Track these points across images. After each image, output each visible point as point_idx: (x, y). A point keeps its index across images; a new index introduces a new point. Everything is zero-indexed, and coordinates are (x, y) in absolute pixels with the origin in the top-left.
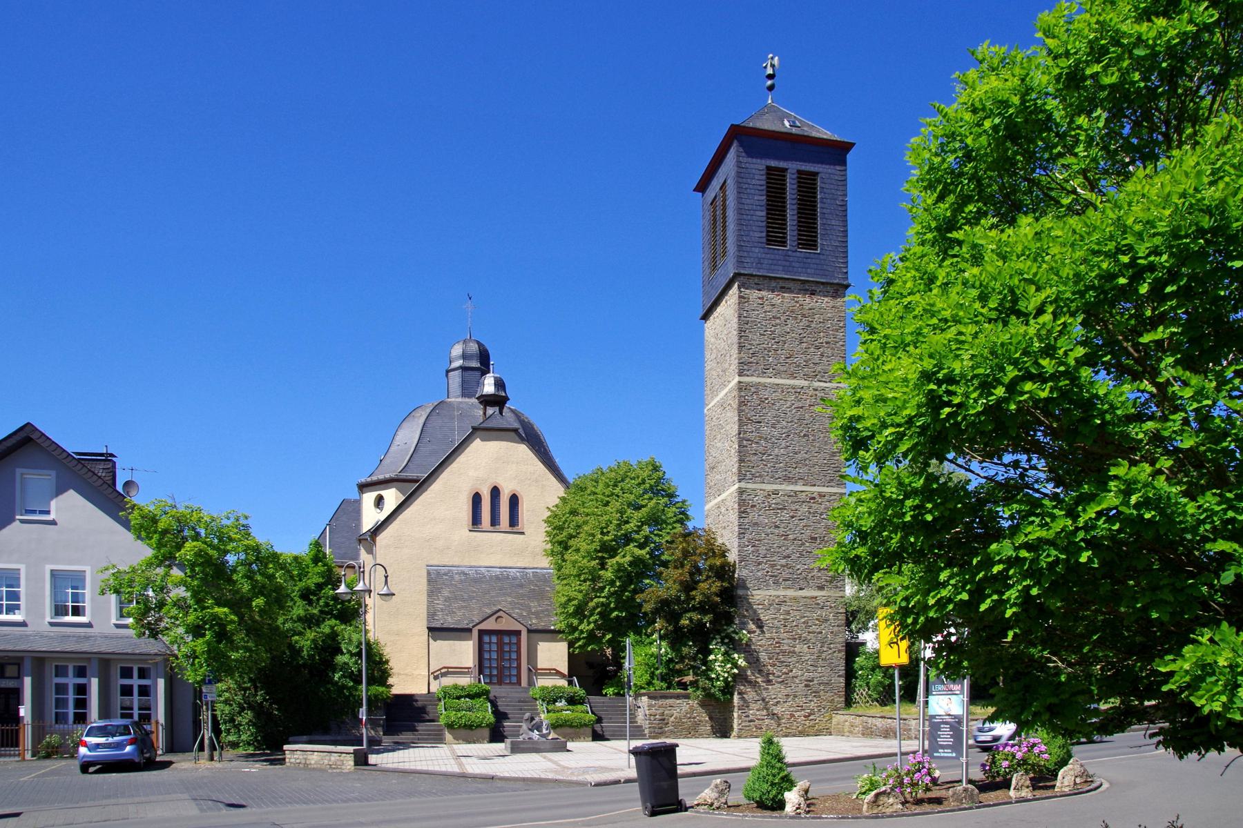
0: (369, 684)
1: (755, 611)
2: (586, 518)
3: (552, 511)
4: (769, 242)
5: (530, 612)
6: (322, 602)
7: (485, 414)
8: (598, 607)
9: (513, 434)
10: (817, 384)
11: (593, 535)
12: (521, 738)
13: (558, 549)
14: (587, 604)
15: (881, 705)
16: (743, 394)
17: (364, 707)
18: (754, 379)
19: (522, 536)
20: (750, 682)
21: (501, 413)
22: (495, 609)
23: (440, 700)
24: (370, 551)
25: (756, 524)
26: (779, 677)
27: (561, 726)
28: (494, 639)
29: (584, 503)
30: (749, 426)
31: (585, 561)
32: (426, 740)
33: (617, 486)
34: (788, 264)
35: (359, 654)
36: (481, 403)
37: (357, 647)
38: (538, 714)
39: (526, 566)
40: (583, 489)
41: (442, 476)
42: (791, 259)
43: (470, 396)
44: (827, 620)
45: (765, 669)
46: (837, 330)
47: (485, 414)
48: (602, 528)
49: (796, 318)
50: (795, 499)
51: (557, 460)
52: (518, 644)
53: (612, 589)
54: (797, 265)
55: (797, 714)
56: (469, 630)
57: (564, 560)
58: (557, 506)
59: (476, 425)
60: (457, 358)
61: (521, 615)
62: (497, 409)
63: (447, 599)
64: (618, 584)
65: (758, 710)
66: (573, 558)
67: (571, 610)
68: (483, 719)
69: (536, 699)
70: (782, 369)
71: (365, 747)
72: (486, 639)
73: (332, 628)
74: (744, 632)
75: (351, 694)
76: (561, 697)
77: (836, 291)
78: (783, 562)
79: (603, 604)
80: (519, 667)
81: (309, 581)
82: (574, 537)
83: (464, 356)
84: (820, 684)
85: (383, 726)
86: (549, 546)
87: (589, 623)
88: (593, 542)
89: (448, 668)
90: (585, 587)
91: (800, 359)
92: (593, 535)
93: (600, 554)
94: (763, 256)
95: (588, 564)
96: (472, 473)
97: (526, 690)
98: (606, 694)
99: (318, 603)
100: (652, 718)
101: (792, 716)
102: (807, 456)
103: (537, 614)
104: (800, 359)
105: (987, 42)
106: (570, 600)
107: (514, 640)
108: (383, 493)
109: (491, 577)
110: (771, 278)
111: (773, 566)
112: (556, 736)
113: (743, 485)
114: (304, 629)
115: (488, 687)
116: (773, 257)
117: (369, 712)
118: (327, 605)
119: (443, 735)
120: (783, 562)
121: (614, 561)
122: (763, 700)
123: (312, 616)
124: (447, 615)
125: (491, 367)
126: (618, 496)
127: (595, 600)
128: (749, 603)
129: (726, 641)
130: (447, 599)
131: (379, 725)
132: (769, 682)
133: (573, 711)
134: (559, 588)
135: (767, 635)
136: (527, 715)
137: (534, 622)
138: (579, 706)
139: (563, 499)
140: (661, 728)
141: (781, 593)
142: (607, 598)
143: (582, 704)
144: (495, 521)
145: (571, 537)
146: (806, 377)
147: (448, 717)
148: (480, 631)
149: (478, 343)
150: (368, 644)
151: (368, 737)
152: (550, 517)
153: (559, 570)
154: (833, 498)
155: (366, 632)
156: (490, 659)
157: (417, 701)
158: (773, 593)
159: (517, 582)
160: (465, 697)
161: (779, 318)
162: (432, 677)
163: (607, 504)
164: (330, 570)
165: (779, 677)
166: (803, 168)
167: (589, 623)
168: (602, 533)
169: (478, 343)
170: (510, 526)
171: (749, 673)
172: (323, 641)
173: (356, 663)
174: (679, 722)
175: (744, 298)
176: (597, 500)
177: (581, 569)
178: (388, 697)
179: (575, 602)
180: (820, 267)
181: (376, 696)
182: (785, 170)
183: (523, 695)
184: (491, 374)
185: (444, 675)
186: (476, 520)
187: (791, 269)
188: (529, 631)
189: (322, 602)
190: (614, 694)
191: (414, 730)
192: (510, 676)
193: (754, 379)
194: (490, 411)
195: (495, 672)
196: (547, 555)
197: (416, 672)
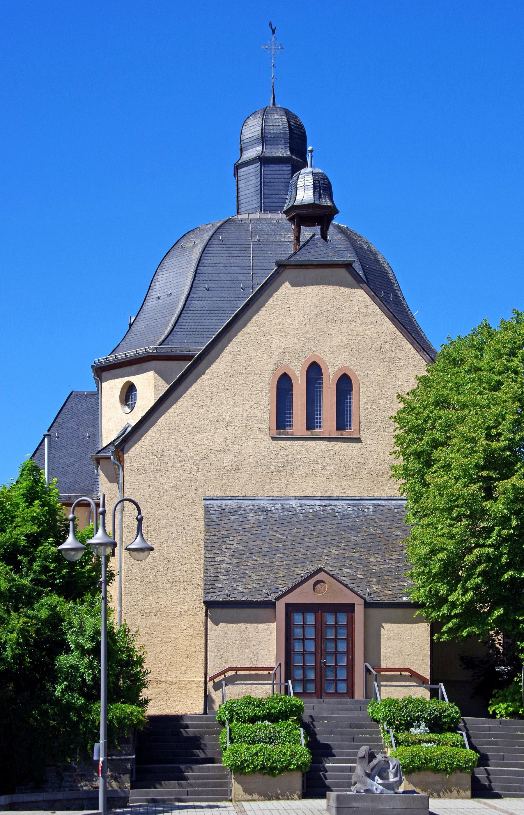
0: (110, 700)
2: (460, 413)
3: (405, 401)
5: (369, 574)
6: (36, 566)
7: (298, 238)
8: (479, 563)
9: (343, 272)
11: (474, 441)
12: (353, 791)
13: (415, 464)
14: (461, 558)
17: (102, 741)
19: (357, 445)
21: (324, 236)
22: (313, 568)
23: (223, 724)
24: (114, 478)
27: (420, 769)
28: (311, 619)
29: (458, 386)
31: (460, 484)
32: (199, 796)
33: (515, 355)
35: (96, 651)
36: (291, 220)
37: (93, 639)
38: (382, 747)
39: (364, 494)
40: (456, 362)
41: (271, 301)
43: (273, 210)
47: (298, 238)
48: (488, 428)
51: (416, 313)
52: (350, 627)
53: (504, 532)
56: (271, 605)
57: (425, 485)
58: (413, 393)
59: (283, 259)
60: (252, 143)
61: (354, 578)
63: (236, 554)
64: (514, 523)
66: (440, 481)
67: (436, 568)
68: (292, 756)
69: (377, 721)
71: (100, 810)
72: (298, 618)
73: (52, 608)
75: (81, 719)
76: (418, 719)
79: (488, 558)
80: (350, 668)
81: (17, 531)
82: (442, 444)
85: (131, 773)
86: (400, 461)
87: (465, 591)
88: (473, 452)
89: (236, 669)
90: (460, 528)
92: (474, 441)
93: (484, 473)
95: (464, 491)
96: (276, 342)
97: (362, 706)
98: (494, 714)
99: (30, 569)
103: (379, 576)
105: (12, 567)
106: (433, 552)
107: (343, 620)
108: (134, 379)
112: (411, 788)
114: (8, 612)
115: (299, 701)
117: (110, 748)
118: (45, 569)
119: (227, 784)
121: (508, 483)
123: (21, 589)
124: (235, 580)
125: (309, 155)
126: (516, 373)
127: (476, 551)
130: (236, 554)
131: (125, 772)
133: (439, 743)
134: (414, 531)
136: (363, 750)
138: (449, 735)
139: (424, 381)
142: (496, 547)
143: (453, 730)
145: (436, 444)
147: (235, 753)
148: (287, 605)
149: (287, 113)
150: (110, 634)
151: (106, 791)
152: (403, 411)
153: (416, 501)
155: (107, 612)
156: (304, 653)
157: (187, 727)
159: (348, 523)
160: (264, 718)
162: (210, 685)
163: (497, 386)
164: (52, 512)
167: (465, 591)
168: (489, 437)
169: (287, 113)
170: (308, 428)
172: (37, 631)
173: (90, 666)
176: (480, 380)
177: (453, 499)
178: (140, 722)
179: (443, 555)
181: (120, 721)
183: (357, 714)
184: (309, 169)
185: (230, 681)
188: (367, 605)
189: (36, 566)
190: (508, 715)
191: (180, 777)
192: (336, 681)
194: (306, 233)
195: (311, 675)
196: (398, 476)
197: (187, 677)
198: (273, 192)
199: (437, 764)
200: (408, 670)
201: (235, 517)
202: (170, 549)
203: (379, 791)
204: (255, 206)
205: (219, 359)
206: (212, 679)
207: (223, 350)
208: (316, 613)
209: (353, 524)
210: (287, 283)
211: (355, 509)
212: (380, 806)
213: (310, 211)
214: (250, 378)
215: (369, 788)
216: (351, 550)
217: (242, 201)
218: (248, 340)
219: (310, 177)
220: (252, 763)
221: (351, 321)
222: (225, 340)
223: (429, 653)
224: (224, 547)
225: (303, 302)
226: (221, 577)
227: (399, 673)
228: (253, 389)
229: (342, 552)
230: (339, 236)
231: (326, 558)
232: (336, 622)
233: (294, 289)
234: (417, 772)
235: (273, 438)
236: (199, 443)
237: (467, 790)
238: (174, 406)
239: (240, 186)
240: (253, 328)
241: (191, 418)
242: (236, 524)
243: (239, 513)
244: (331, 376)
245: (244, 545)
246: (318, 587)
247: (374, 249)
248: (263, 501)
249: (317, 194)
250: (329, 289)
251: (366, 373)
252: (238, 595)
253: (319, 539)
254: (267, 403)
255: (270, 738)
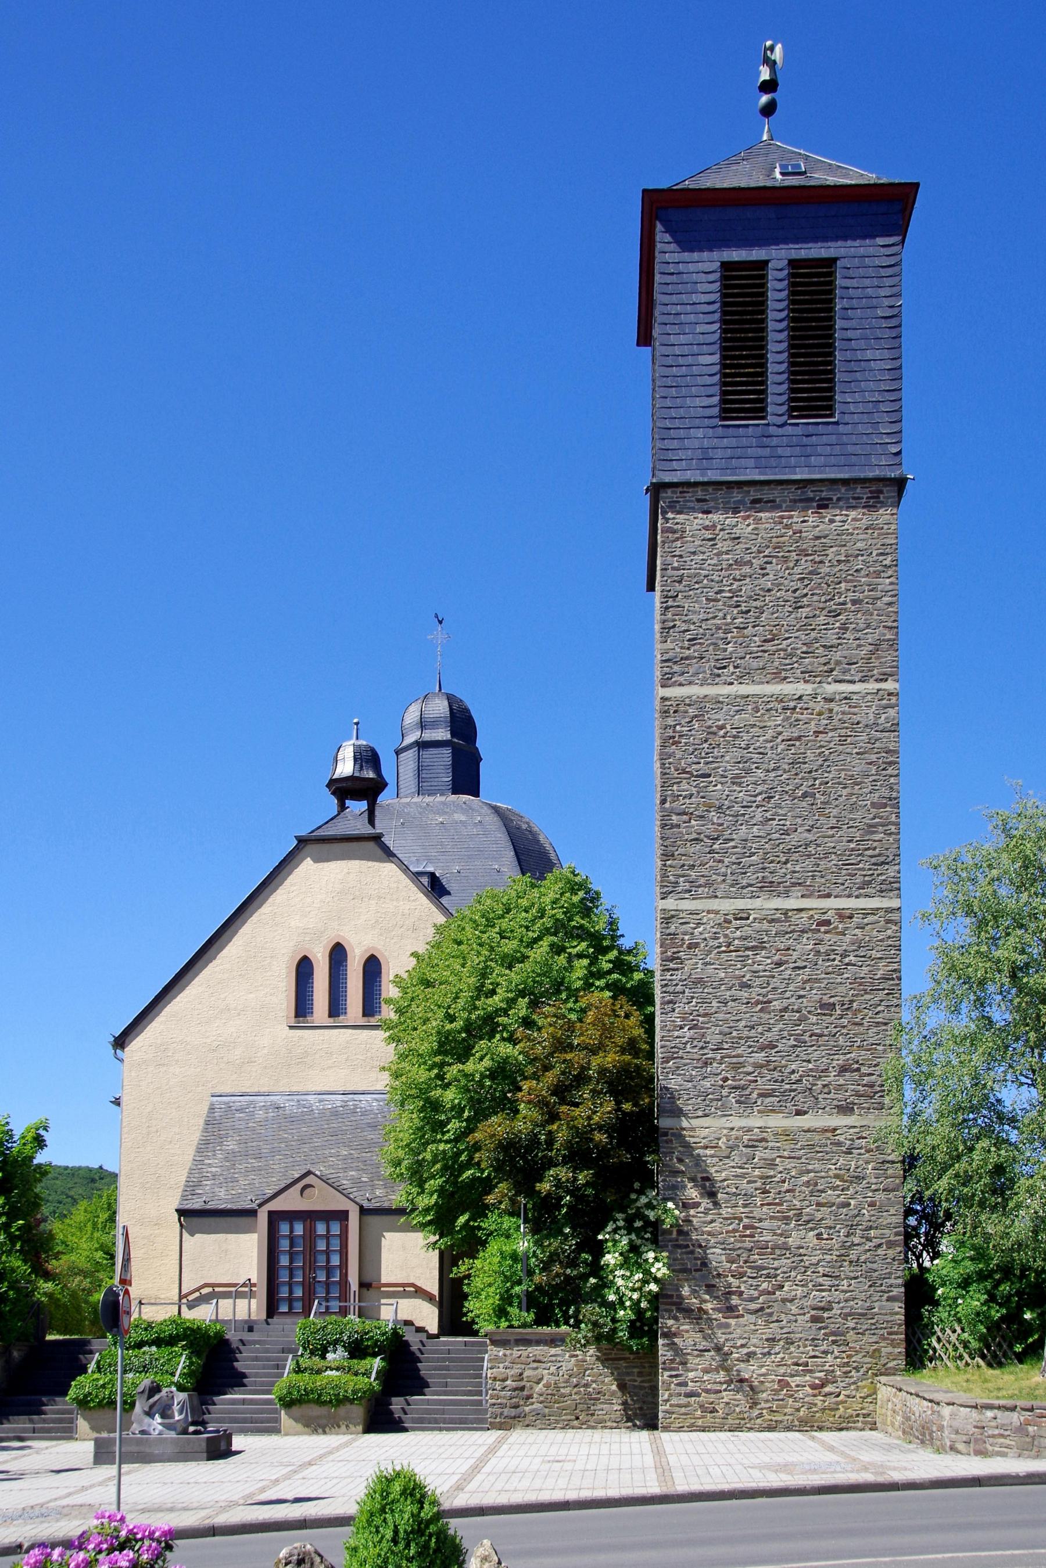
1: (698, 1160)
4: (726, 413)
9: (371, 845)
10: (830, 688)
15: (990, 1365)
16: (670, 721)
18: (695, 691)
20: (688, 1312)
25: (700, 981)
26: (752, 1300)
28: (299, 1229)
30: (684, 785)
34: (767, 452)
42: (774, 441)
44: (860, 1178)
45: (720, 1283)
46: (878, 574)
49: (786, 559)
50: (785, 927)
54: (788, 452)
55: (794, 1381)
59: (303, 832)
62: (363, 805)
65: (706, 1371)
70: (755, 664)
74: (670, 1205)
76: (336, 1342)
77: (876, 495)
78: (760, 1057)
83: (423, 724)
84: (845, 1317)
89: (213, 1285)
91: (797, 642)
94: (716, 442)
100: (498, 1385)
101: (783, 1384)
102: (810, 837)
104: (797, 642)
107: (336, 1229)
109: (322, 1112)
110: (729, 485)
111: (736, 1067)
113: (670, 903)
116: (733, 442)
119: (277, 1420)
120: (760, 1057)
122: (718, 1349)
128: (687, 1146)
129: (638, 1224)
132: (730, 1310)
135: (725, 1212)
137: (364, 1197)
140: (516, 1407)
141: (756, 1121)
144: (336, 1008)
146: (808, 675)
148: (270, 1213)
149: (451, 699)
154: (870, 919)
158: (737, 1122)
159: (368, 1119)
160: (150, 1344)
161: (750, 563)
165: (752, 1300)
166: (794, 255)
170: (365, 1015)
171: (686, 1291)
174: (554, 1394)
175: (674, 532)
180: (837, 449)
182: (763, 264)
186: (302, 1007)
187: (773, 462)
188: (363, 1211)
193: (695, 691)
198: (431, 776)
199: (320, 1395)
200: (412, 1285)
201: (241, 1115)
202: (172, 1151)
203: (157, 1432)
204: (413, 790)
205: (231, 943)
206: (186, 1296)
207: (237, 932)
208: (304, 1222)
209: (375, 1120)
210: (309, 859)
211: (381, 1103)
212: (148, 1450)
213: (350, 784)
214: (266, 963)
215: (145, 1428)
216: (364, 1150)
217: (401, 787)
218: (264, 921)
219: (351, 749)
220: (97, 1396)
221: (380, 898)
222: (238, 922)
223: (438, 1265)
224: (218, 1148)
225: (326, 878)
226: (205, 1182)
227: (402, 1289)
228: (269, 974)
229: (352, 1152)
230: (492, 815)
231: (331, 1159)
232: (328, 1231)
233: (316, 865)
234: (298, 1405)
235: (291, 1027)
236: (208, 1034)
237: (358, 1424)
238: (181, 995)
239: (400, 771)
240: (270, 908)
241: (200, 1006)
242: (240, 1122)
243: (247, 1110)
244: (357, 958)
245: (241, 1146)
246: (307, 1191)
247: (536, 829)
248: (278, 1097)
249: (357, 766)
250: (355, 865)
251: (396, 954)
252: (218, 1202)
253: (330, 1138)
254: (284, 989)
255: (144, 1367)
